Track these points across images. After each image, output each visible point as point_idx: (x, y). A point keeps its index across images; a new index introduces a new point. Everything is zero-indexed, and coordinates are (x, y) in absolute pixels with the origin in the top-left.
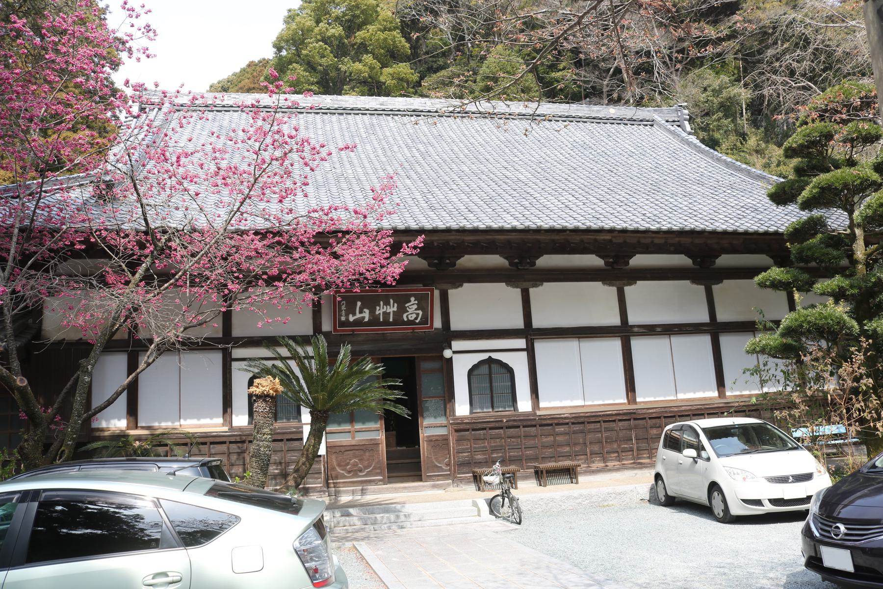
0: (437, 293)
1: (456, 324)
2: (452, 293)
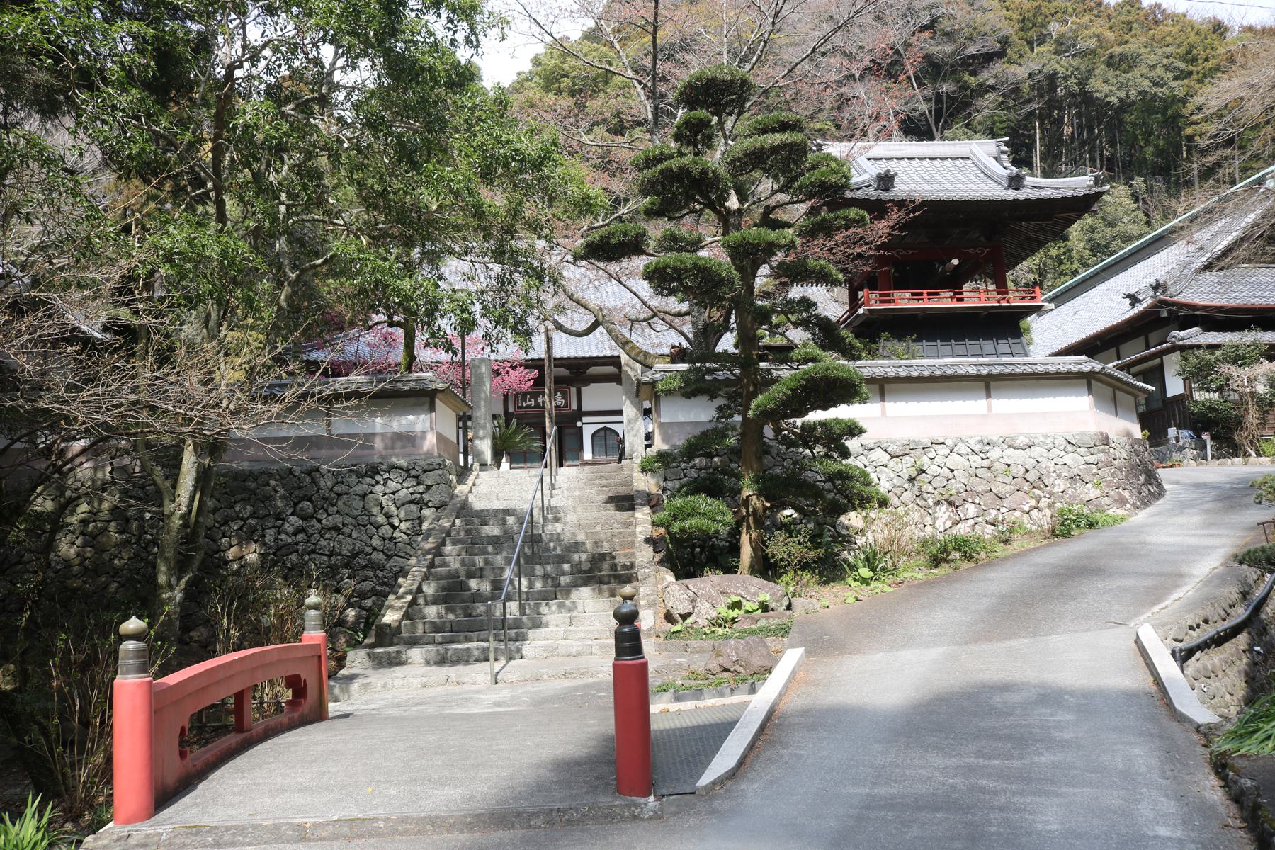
0: (574, 390)
1: (585, 408)
2: (583, 389)
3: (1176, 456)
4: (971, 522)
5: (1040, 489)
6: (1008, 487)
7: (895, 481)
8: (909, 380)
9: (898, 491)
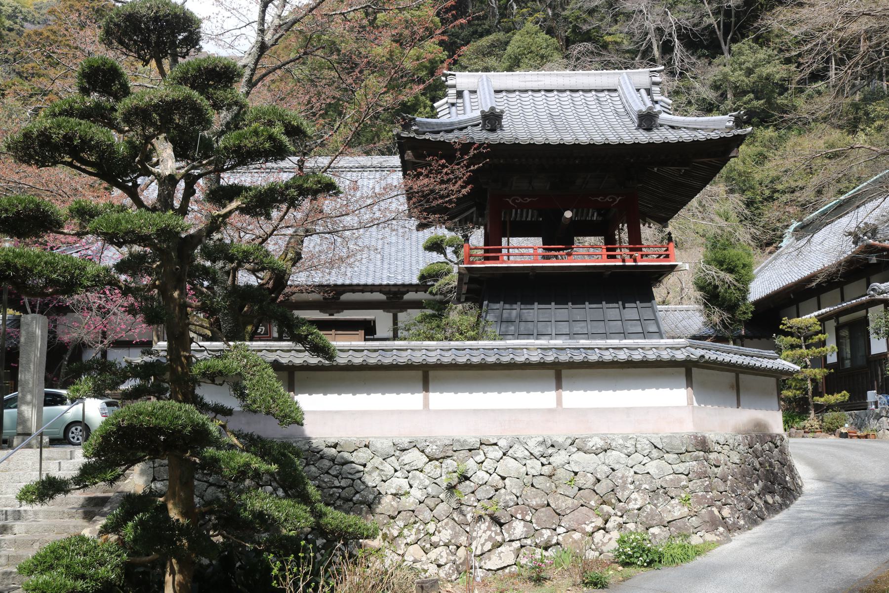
3: (873, 424)
4: (517, 544)
5: (610, 504)
6: (570, 501)
7: (429, 489)
8: (454, 366)
9: (431, 502)
